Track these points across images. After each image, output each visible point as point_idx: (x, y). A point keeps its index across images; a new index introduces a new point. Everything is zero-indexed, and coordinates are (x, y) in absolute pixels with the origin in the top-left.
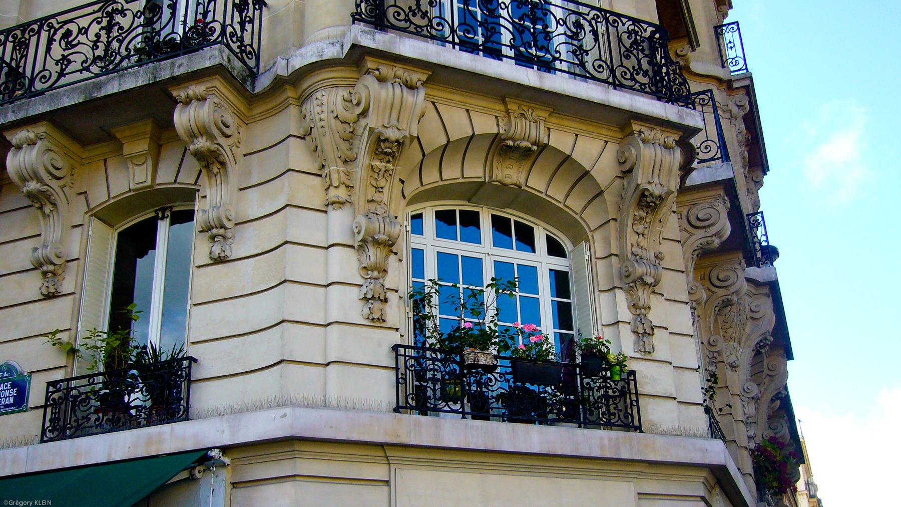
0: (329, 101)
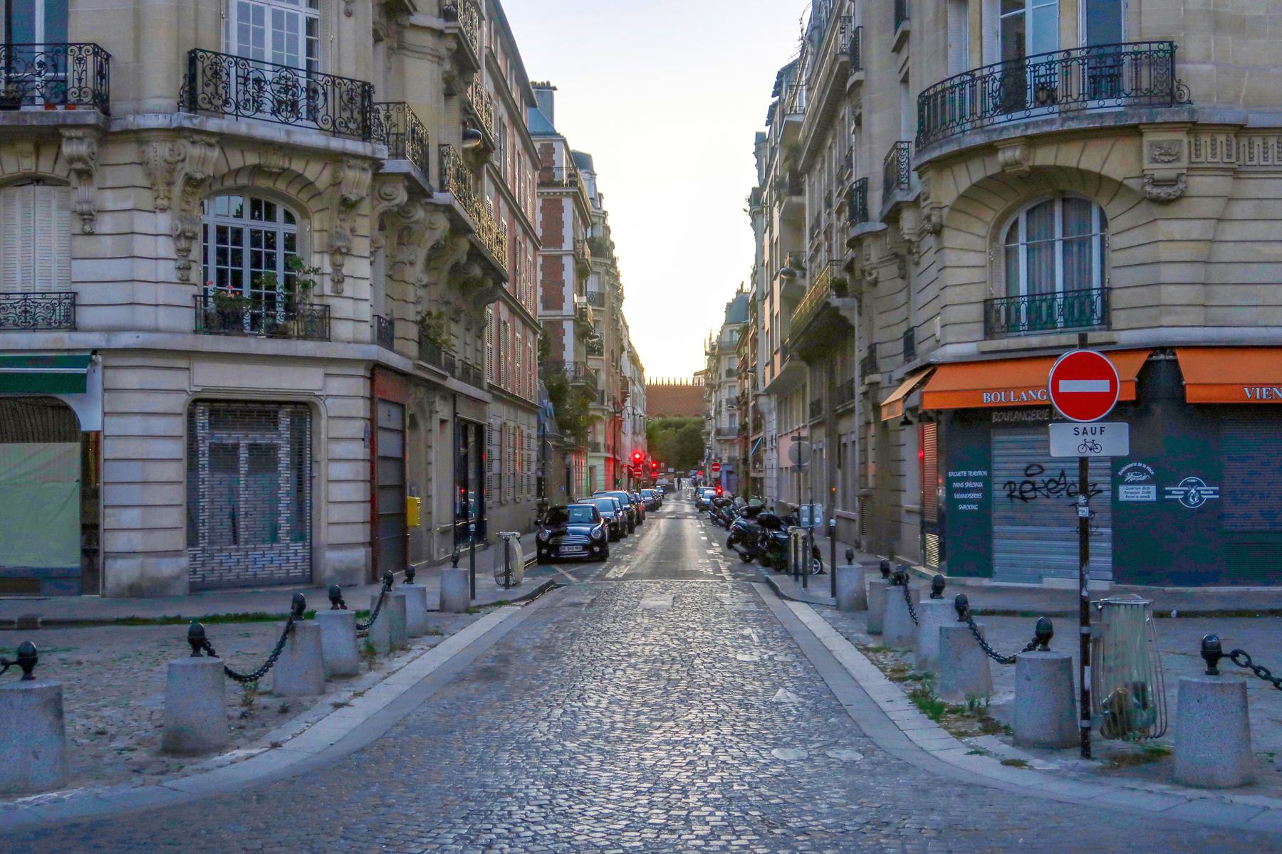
0: (160, 151)
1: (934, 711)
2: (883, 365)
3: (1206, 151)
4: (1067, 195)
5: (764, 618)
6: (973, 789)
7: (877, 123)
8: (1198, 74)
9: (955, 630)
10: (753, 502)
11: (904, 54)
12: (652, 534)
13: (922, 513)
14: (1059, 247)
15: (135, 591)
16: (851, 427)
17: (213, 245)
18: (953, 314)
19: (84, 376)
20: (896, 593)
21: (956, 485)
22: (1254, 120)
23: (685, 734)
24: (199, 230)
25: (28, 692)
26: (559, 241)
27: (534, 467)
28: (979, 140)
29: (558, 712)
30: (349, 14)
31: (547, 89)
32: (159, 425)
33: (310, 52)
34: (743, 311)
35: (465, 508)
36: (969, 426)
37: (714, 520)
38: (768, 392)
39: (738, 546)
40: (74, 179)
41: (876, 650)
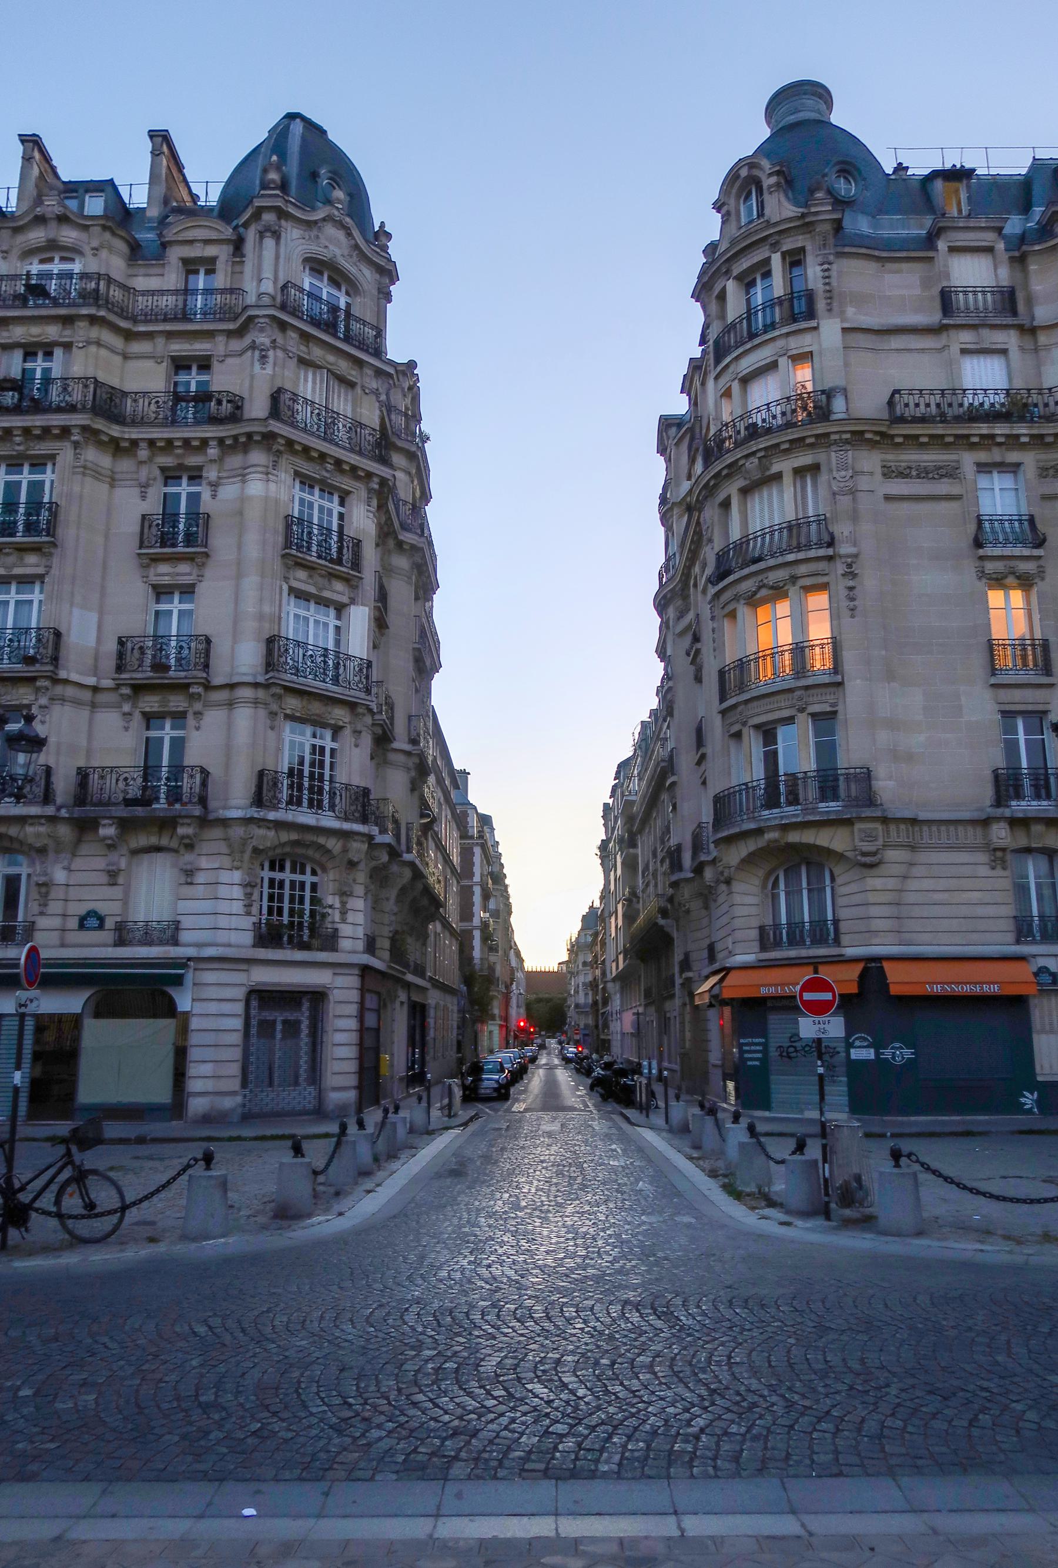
0: (237, 832)
1: (737, 1195)
2: (696, 966)
3: (893, 833)
4: (810, 861)
5: (624, 1139)
6: (761, 1236)
7: (686, 808)
8: (885, 786)
9: (748, 1144)
10: (607, 1059)
11: (703, 767)
12: (536, 1080)
13: (723, 1066)
14: (805, 893)
15: (207, 1119)
16: (674, 1006)
17: (266, 891)
18: (739, 935)
19: (181, 976)
20: (709, 1121)
21: (746, 1048)
22: (922, 816)
23: (587, 1208)
24: (259, 881)
25: (210, 1177)
26: (472, 875)
27: (455, 1032)
28: (752, 826)
29: (506, 1196)
30: (357, 746)
31: (465, 774)
32: (227, 1008)
33: (331, 769)
34: (593, 920)
35: (413, 1062)
36: (752, 1011)
37: (578, 1071)
38: (614, 980)
39: (599, 1089)
40: (182, 850)
41: (699, 1159)
